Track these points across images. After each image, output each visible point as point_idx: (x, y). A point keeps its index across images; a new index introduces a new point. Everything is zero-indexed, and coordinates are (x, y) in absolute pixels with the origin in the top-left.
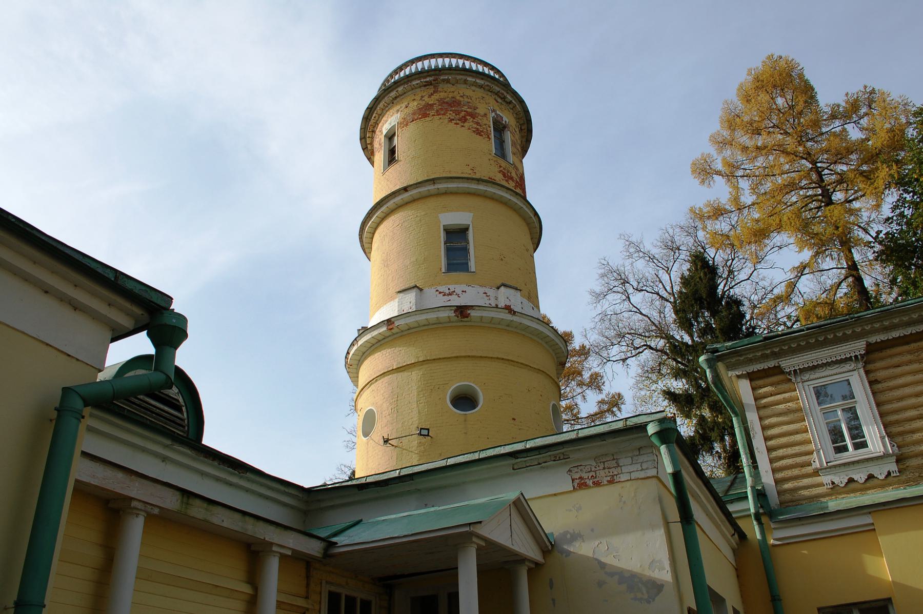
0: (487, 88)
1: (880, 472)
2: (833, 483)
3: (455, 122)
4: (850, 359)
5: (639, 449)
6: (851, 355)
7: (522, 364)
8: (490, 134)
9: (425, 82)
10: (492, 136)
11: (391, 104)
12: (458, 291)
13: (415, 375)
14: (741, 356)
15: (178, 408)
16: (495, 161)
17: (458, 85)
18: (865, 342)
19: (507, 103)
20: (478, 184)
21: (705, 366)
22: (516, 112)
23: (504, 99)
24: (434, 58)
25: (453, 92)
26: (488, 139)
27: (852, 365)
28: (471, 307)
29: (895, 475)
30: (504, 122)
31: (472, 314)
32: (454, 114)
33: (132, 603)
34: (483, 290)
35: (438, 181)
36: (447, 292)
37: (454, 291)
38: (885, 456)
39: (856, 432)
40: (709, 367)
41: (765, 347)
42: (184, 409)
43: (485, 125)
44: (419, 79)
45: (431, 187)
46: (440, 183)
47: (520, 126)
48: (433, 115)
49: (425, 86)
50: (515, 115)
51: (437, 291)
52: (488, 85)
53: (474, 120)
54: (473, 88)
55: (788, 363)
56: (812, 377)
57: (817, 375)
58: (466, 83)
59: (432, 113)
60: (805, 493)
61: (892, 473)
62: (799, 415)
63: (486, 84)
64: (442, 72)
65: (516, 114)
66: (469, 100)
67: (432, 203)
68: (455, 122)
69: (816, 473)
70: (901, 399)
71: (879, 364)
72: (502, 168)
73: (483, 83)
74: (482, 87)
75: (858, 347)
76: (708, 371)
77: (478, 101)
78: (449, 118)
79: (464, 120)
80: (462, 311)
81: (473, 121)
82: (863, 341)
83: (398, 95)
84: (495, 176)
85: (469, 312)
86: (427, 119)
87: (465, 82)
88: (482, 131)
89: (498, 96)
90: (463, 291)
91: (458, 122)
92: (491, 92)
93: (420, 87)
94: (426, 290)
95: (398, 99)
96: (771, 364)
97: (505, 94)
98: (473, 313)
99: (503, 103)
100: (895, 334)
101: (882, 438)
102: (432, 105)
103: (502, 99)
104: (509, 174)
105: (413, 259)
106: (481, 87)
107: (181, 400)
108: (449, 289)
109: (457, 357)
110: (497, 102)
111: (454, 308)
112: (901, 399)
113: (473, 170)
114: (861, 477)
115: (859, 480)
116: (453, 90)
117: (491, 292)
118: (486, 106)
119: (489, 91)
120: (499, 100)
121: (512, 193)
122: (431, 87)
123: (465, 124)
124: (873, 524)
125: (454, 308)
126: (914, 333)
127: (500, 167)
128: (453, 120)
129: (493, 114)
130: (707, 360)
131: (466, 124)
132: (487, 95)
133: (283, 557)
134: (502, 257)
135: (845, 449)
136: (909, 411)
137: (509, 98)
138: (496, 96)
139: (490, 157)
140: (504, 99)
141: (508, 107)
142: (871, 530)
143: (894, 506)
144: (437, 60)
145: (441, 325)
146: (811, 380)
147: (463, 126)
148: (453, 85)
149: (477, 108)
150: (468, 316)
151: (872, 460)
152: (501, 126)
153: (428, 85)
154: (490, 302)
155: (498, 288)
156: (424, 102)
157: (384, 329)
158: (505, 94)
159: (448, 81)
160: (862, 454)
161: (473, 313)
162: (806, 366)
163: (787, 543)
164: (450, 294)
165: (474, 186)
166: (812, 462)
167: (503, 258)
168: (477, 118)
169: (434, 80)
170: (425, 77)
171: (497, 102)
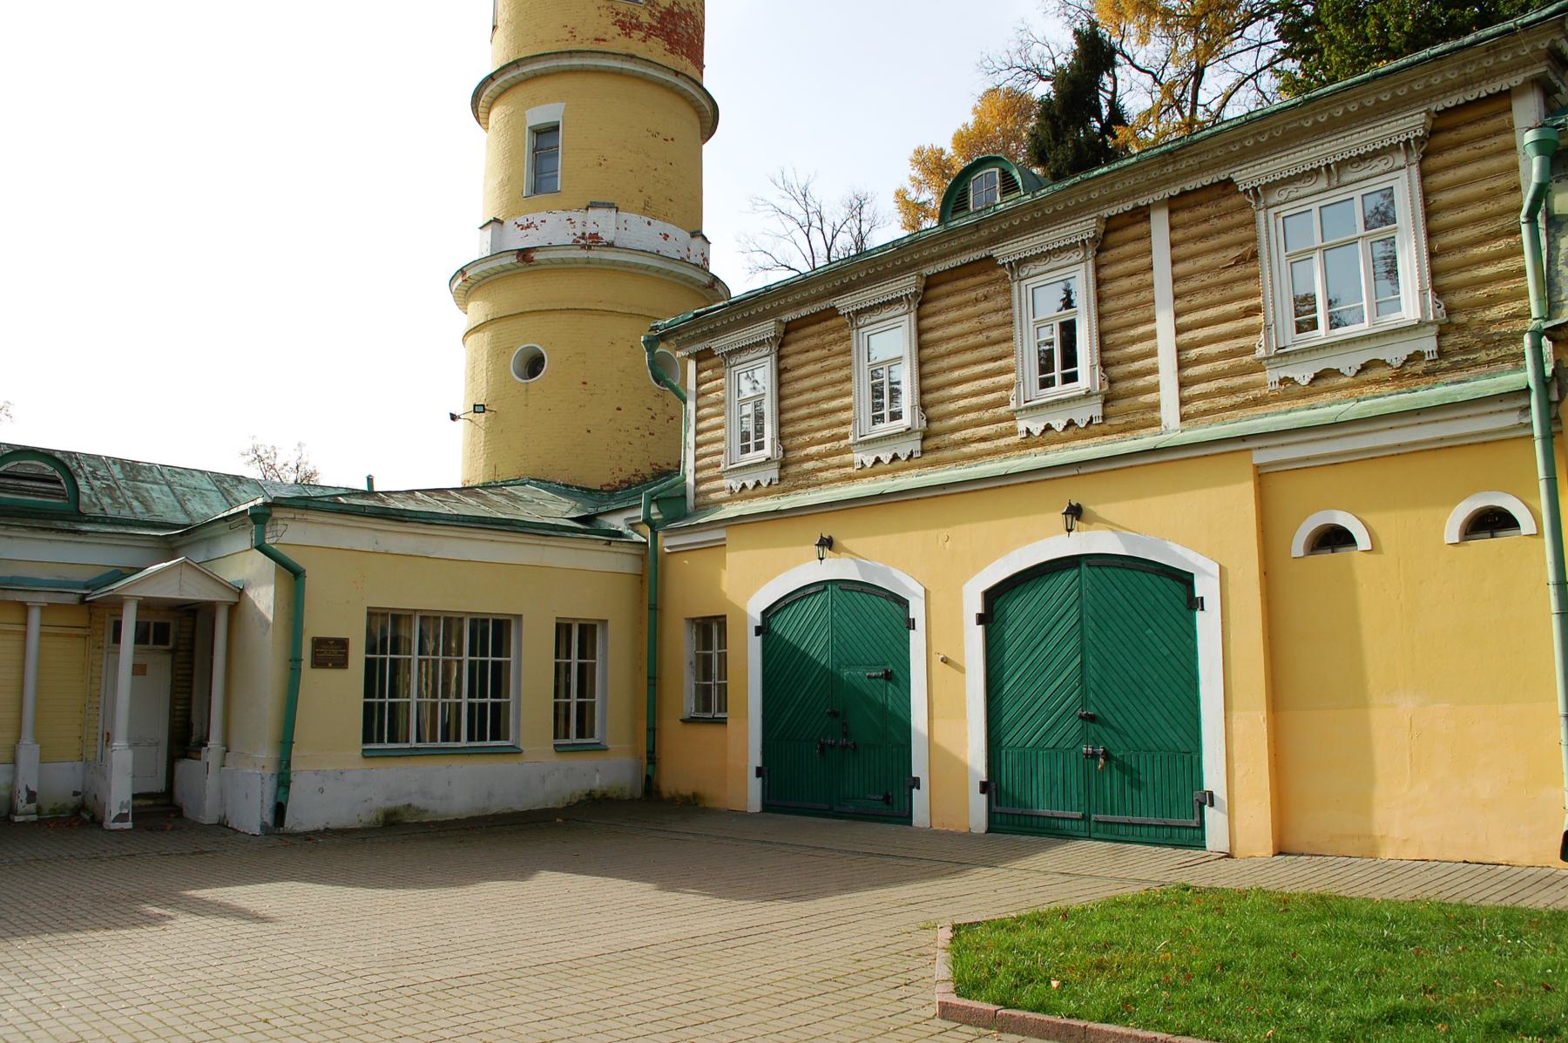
2: (1028, 431)
4: (1316, 172)
6: (1409, 136)
12: (537, 222)
13: (484, 337)
14: (679, 335)
15: (58, 482)
18: (1424, 114)
27: (1075, 257)
28: (534, 249)
29: (1431, 358)
31: (535, 258)
33: (42, 625)
35: (522, 63)
36: (525, 224)
38: (1421, 325)
39: (1070, 359)
41: (698, 325)
42: (62, 481)
45: (515, 73)
55: (1005, 252)
57: (743, 359)
60: (713, 496)
62: (1252, 269)
67: (521, 93)
69: (1011, 417)
80: (524, 254)
82: (1420, 113)
94: (506, 222)
96: (981, 254)
98: (537, 256)
100: (804, 312)
101: (1422, 293)
104: (634, 21)
105: (500, 179)
107: (58, 475)
109: (522, 313)
114: (1059, 424)
115: (1347, 372)
117: (578, 217)
124: (724, 539)
126: (1484, 98)
133: (42, 608)
135: (1314, 325)
142: (720, 545)
143: (837, 508)
145: (510, 273)
146: (1033, 276)
150: (531, 260)
154: (574, 230)
155: (587, 209)
157: (460, 281)
160: (1071, 389)
161: (537, 256)
162: (1067, 243)
163: (677, 551)
164: (528, 227)
165: (566, 62)
166: (1257, 346)
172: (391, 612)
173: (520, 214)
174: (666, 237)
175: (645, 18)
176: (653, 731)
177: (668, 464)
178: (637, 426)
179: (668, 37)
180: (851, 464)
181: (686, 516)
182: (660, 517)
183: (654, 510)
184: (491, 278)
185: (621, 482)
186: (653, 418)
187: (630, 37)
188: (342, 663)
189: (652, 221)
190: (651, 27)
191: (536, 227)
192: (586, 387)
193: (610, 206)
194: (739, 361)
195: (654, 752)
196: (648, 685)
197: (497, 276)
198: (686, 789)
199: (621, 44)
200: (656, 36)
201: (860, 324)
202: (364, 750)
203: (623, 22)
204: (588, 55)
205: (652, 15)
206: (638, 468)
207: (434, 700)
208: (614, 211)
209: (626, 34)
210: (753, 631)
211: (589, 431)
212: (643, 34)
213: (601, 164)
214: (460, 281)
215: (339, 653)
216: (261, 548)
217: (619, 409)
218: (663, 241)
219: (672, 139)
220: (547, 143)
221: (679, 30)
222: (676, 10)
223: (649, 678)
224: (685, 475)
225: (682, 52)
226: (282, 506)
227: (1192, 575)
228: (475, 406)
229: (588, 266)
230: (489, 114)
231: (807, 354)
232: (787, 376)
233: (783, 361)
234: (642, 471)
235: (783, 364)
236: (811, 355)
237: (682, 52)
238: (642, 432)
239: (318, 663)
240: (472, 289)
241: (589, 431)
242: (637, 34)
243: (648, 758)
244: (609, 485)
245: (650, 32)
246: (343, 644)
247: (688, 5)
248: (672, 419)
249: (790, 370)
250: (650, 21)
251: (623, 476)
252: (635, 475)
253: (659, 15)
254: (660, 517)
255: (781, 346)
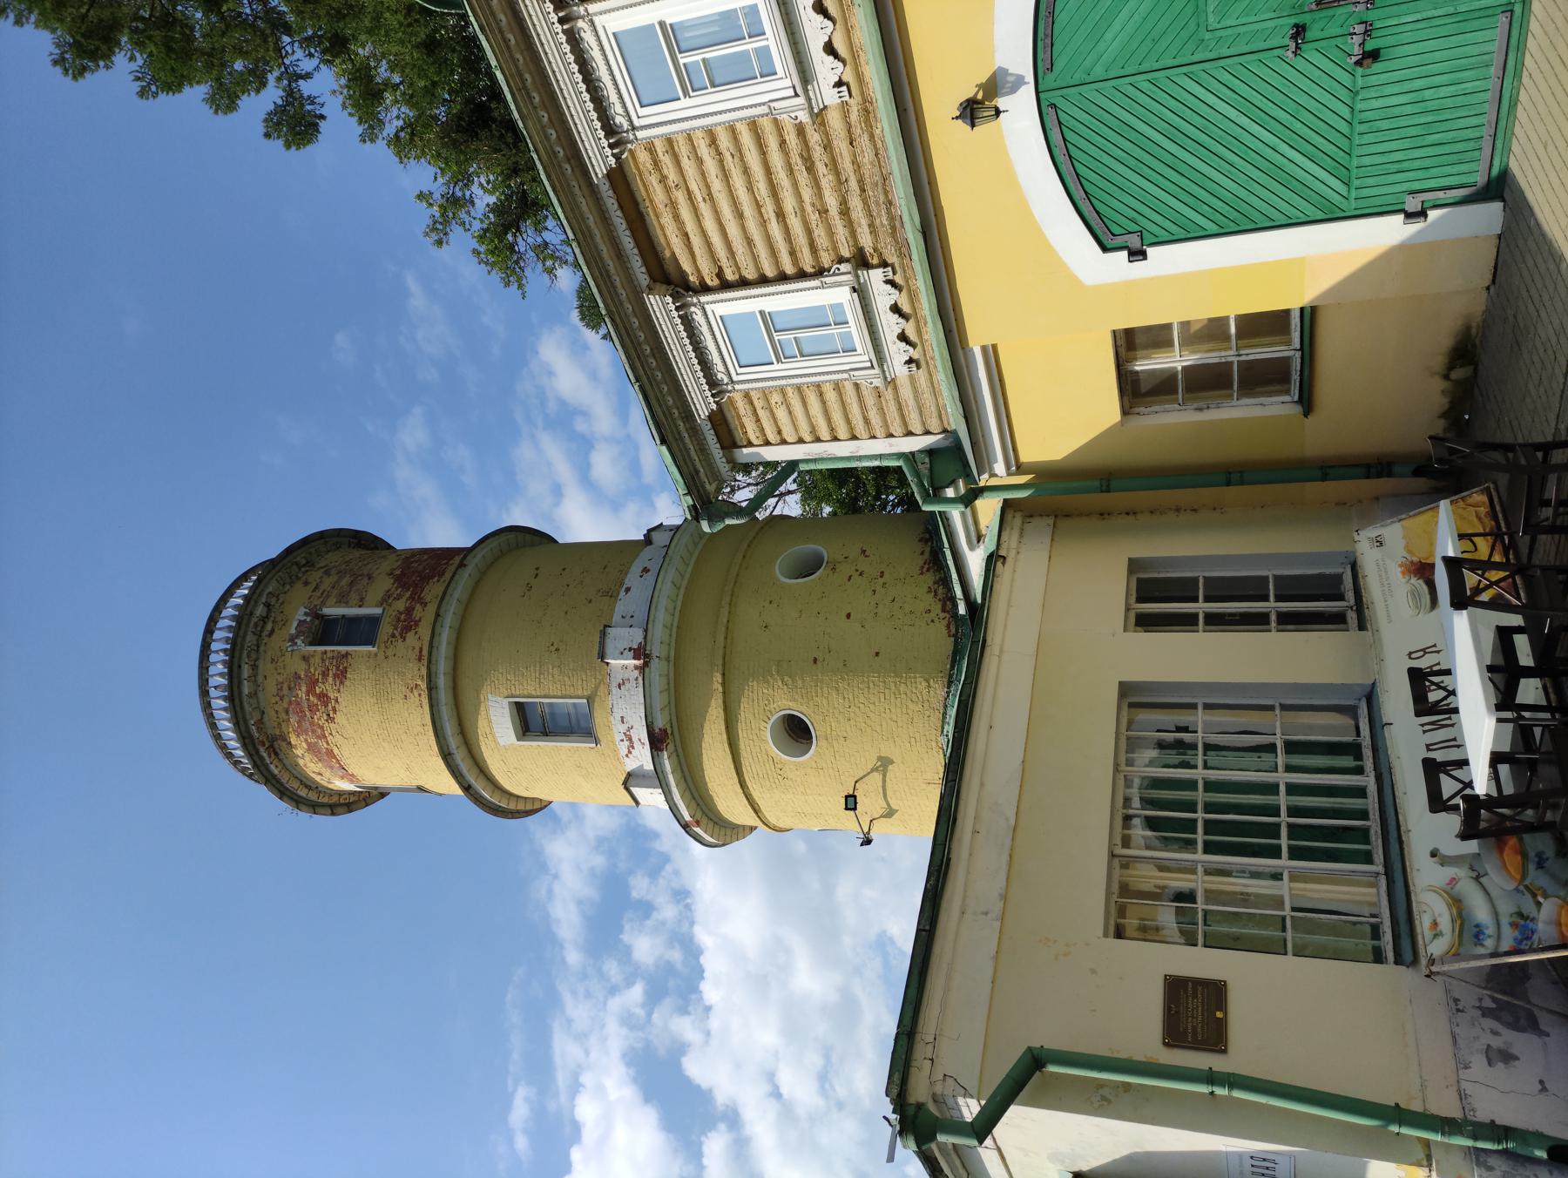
0: (254, 656)
1: (883, 297)
3: (331, 713)
5: (932, 1060)
7: (726, 638)
8: (339, 652)
9: (270, 757)
10: (343, 649)
11: (320, 789)
12: (623, 728)
16: (386, 647)
17: (262, 705)
19: (269, 611)
20: (436, 688)
21: (719, 526)
22: (281, 588)
23: (264, 619)
24: (207, 680)
25: (277, 712)
26: (349, 657)
30: (308, 619)
31: (661, 726)
32: (318, 713)
34: (615, 690)
35: (445, 748)
37: (624, 733)
40: (722, 519)
43: (323, 661)
44: (267, 767)
46: (448, 746)
47: (303, 569)
48: (328, 744)
49: (276, 754)
50: (288, 587)
51: (627, 756)
52: (248, 656)
53: (320, 680)
54: (260, 678)
56: (720, 367)
58: (256, 694)
59: (322, 744)
61: (887, 278)
63: (247, 660)
64: (245, 734)
65: (283, 585)
66: (285, 686)
68: (331, 713)
70: (749, 242)
71: (687, 266)
72: (395, 632)
73: (246, 666)
74: (255, 665)
75: (660, 307)
76: (729, 522)
77: (282, 671)
78: (327, 720)
79: (324, 698)
81: (323, 683)
83: (301, 787)
84: (414, 648)
85: (657, 730)
86: (336, 751)
87: (253, 695)
88: (338, 669)
89: (261, 632)
90: (623, 722)
91: (330, 708)
92: (258, 647)
93: (280, 760)
95: (309, 783)
97: (254, 620)
99: (272, 619)
100: (628, 243)
102: (309, 744)
103: (265, 623)
104: (403, 617)
106: (254, 667)
108: (622, 740)
110: (273, 631)
111: (655, 753)
112: (749, 242)
113: (412, 688)
116: (273, 714)
118: (288, 655)
119: (257, 651)
120: (269, 627)
121: (438, 624)
122: (276, 746)
123: (332, 697)
125: (655, 753)
127: (393, 636)
128: (328, 715)
129: (299, 642)
130: (711, 521)
131: (332, 695)
132: (265, 652)
134: (553, 648)
136: (771, 233)
137: (260, 610)
138: (264, 634)
139: (381, 655)
140: (264, 619)
141: (277, 606)
144: (213, 652)
147: (337, 701)
148: (263, 712)
149: (296, 673)
151: (866, 305)
152: (317, 622)
153: (274, 750)
156: (306, 754)
158: (254, 620)
159: (260, 722)
164: (630, 739)
167: (555, 647)
168: (314, 675)
169: (263, 745)
170: (262, 758)
171: (273, 631)
172: (1115, 898)
173: (615, 751)
174: (646, 570)
175: (401, 605)
176: (1326, 469)
177: (922, 553)
178: (871, 593)
179: (426, 579)
180: (844, 108)
181: (958, 447)
182: (961, 483)
183: (950, 493)
184: (692, 787)
185: (944, 610)
186: (861, 575)
187: (420, 620)
188: (1215, 992)
189: (625, 586)
190: (411, 598)
191: (629, 729)
192: (820, 659)
193: (603, 634)
194: (720, 367)
195: (1368, 466)
196: (1242, 483)
197: (689, 779)
198: (1433, 395)
199: (424, 630)
200: (421, 593)
201: (626, 126)
202: (1397, 962)
203: (402, 630)
204: (433, 668)
205: (399, 598)
206: (926, 589)
207: (1284, 832)
208: (609, 630)
209: (416, 625)
210: (1139, 265)
211: (877, 654)
212: (418, 607)
213: (557, 650)
214: (698, 830)
215: (1195, 995)
216: (983, 1128)
217: (848, 616)
218: (650, 573)
219: (537, 569)
220: (535, 721)
221: (420, 568)
222: (398, 572)
223: (1228, 484)
224: (900, 456)
225: (445, 564)
226: (904, 1081)
227: (1114, 332)
228: (847, 809)
229: (677, 663)
230: (518, 797)
231: (691, 236)
232: (730, 276)
233: (709, 283)
234: (931, 583)
235: (712, 282)
236: (690, 227)
237: (445, 564)
238: (879, 589)
239: (1215, 1039)
240: (709, 814)
241: (877, 654)
242: (417, 613)
243: (1379, 475)
244: (948, 626)
245: (417, 598)
246: (1176, 988)
247: (397, 561)
248: (864, 552)
249: (720, 268)
250: (404, 599)
251: (937, 608)
252: (936, 595)
253: (400, 589)
254: (961, 483)
255: (688, 288)
